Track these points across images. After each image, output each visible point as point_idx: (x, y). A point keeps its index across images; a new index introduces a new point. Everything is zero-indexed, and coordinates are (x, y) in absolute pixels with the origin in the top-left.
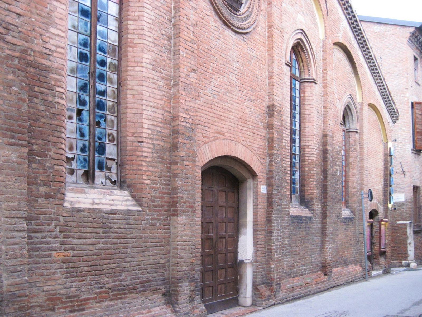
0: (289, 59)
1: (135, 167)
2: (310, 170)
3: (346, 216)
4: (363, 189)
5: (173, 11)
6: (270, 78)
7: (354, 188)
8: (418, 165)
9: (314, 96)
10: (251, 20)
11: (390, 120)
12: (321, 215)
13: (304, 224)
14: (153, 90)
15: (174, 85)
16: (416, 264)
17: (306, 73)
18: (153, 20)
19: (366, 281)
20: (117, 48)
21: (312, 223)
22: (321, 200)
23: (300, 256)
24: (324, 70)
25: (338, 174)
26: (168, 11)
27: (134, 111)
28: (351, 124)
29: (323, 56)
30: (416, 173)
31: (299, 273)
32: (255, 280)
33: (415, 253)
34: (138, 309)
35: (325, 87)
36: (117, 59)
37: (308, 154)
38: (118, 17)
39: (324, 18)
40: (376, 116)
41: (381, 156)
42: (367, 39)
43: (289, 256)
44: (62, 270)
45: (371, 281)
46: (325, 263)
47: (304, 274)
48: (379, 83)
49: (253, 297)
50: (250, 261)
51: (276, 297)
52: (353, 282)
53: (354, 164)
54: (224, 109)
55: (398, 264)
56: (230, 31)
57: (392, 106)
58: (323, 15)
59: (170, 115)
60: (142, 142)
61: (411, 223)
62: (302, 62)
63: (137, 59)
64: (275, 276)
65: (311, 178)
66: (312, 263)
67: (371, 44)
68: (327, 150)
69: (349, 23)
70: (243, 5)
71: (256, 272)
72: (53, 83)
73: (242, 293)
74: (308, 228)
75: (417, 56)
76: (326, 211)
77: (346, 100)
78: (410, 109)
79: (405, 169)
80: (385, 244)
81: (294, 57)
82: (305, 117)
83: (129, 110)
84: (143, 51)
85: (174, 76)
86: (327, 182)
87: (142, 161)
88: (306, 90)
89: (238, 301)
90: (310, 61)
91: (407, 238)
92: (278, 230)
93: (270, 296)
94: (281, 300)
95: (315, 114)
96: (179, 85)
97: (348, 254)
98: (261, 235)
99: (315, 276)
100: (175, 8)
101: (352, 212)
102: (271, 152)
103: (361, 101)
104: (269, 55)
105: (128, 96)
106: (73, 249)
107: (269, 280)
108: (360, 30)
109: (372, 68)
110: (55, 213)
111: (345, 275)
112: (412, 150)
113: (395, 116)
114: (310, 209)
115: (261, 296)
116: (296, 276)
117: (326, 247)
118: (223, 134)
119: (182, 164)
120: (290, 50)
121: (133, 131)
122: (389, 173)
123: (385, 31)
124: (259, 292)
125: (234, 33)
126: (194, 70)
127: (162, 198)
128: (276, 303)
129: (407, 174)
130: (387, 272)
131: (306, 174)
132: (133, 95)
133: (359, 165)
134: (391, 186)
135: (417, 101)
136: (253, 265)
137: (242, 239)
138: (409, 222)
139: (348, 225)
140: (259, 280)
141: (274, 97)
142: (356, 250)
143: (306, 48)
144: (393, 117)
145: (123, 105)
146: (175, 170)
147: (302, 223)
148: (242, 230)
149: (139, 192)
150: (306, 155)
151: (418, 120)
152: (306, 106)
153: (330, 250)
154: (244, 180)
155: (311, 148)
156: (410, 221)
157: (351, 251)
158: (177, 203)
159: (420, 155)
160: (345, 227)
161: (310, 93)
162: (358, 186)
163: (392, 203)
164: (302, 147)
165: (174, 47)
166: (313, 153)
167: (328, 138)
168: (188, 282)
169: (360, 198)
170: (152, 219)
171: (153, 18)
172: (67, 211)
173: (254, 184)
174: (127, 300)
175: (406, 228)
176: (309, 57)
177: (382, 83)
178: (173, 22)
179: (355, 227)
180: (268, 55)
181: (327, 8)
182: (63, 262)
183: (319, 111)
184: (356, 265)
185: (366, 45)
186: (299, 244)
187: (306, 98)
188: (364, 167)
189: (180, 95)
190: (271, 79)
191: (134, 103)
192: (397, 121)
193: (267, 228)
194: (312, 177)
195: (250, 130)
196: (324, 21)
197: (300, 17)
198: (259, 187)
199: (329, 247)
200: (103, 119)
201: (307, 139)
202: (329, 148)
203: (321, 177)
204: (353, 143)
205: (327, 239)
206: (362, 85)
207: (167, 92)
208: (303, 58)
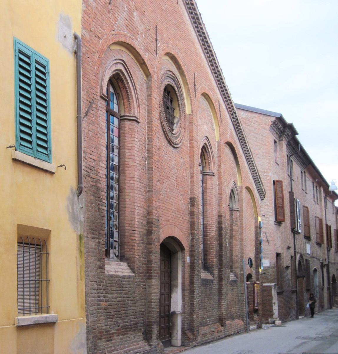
0: (105, 93)
1: (131, 247)
2: (211, 243)
3: (233, 279)
4: (243, 257)
5: (147, 141)
6: (192, 177)
7: (237, 256)
8: (279, 235)
9: (213, 186)
10: (181, 136)
11: (259, 199)
12: (218, 278)
13: (209, 285)
14: (139, 195)
15: (149, 191)
16: (280, 322)
17: (207, 168)
18: (138, 148)
19: (247, 333)
20: (118, 167)
21: (213, 285)
22: (218, 267)
23: (207, 310)
24: (219, 165)
25: (227, 246)
26: (144, 141)
27: (130, 210)
28: (234, 204)
29: (218, 154)
30: (277, 241)
31: (206, 323)
32: (184, 327)
33: (279, 312)
34: (133, 342)
35: (220, 178)
36: (118, 174)
37: (209, 230)
38: (118, 146)
39: (219, 125)
40: (250, 196)
41: (253, 229)
42: (245, 136)
43: (201, 310)
44: (104, 314)
45: (251, 333)
46: (222, 317)
47: (209, 324)
48: (252, 169)
49: (182, 339)
50: (180, 312)
51: (196, 341)
52: (238, 333)
53: (237, 236)
54: (169, 203)
55: (265, 321)
56: (171, 147)
57: (261, 187)
58: (219, 123)
59: (146, 211)
60: (135, 230)
61: (275, 285)
62: (205, 159)
63: (131, 176)
64: (196, 324)
65: (211, 250)
66: (213, 315)
67: (247, 139)
68: (222, 227)
69: (233, 124)
70: (175, 125)
71: (184, 321)
72: (102, 197)
73: (174, 336)
74: (211, 288)
75: (276, 140)
76: (222, 275)
77: (231, 185)
78: (272, 186)
79: (269, 238)
80: (258, 303)
81: (111, 90)
82: (207, 202)
83: (126, 209)
84: (135, 171)
85: (149, 185)
86: (222, 253)
87: (135, 243)
88: (208, 181)
89: (171, 342)
90: (210, 159)
91: (272, 298)
92: (197, 290)
93: (193, 339)
94: (199, 343)
95: (214, 200)
96: (152, 191)
97: (234, 310)
98: (187, 293)
99: (215, 326)
100: (148, 138)
101: (235, 276)
102: (192, 232)
103: (241, 185)
104: (191, 160)
105: (126, 200)
106: (108, 301)
107: (192, 327)
108: (241, 129)
109: (249, 160)
110: (102, 278)
111: (234, 327)
112: (275, 222)
113: (263, 194)
114: (212, 273)
115: (188, 339)
116: (205, 326)
117: (222, 303)
118: (169, 221)
119: (154, 245)
120: (106, 83)
121: (129, 223)
122: (259, 242)
123: (251, 118)
124: (187, 335)
125: (173, 148)
126: (159, 180)
127: (143, 267)
128: (197, 344)
129: (271, 242)
130: (259, 327)
131: (208, 246)
132: (129, 199)
133: (240, 237)
134: (260, 253)
135: (278, 179)
136: (182, 316)
137: (173, 296)
138: (273, 284)
139: (234, 286)
140: (186, 327)
141: (195, 192)
142: (238, 307)
143: (208, 149)
144: (261, 195)
145: (122, 205)
146: (150, 248)
147: (208, 284)
148: (174, 289)
149: (133, 263)
150: (208, 231)
151: (279, 196)
152: (208, 193)
153: (224, 306)
154: (176, 252)
155: (212, 226)
156: (274, 284)
157: (236, 307)
158: (152, 271)
159: (280, 226)
160: (232, 288)
161: (210, 183)
162: (239, 254)
163: (262, 269)
164: (205, 225)
165: (148, 165)
166: (213, 231)
167: (223, 218)
168: (156, 325)
169: (241, 264)
170: (139, 282)
171: (139, 147)
172: (106, 277)
173: (182, 256)
174: (128, 335)
175: (271, 290)
176: (210, 156)
177: (254, 169)
178: (147, 148)
179: (238, 288)
180: (190, 160)
181: (221, 117)
182: (105, 309)
183: (216, 197)
184: (239, 320)
185: (244, 140)
186: (206, 301)
187: (208, 187)
188: (244, 239)
189: (153, 199)
190: (192, 178)
191: (130, 204)
192: (264, 199)
193: (190, 288)
194: (212, 249)
195: (181, 217)
196: (219, 127)
197: (205, 127)
198: (186, 258)
199: (224, 303)
200: (113, 215)
201: (208, 219)
202: (223, 226)
203: (218, 248)
204: (236, 219)
205: (223, 298)
206: (242, 173)
207: (145, 196)
208: (205, 157)
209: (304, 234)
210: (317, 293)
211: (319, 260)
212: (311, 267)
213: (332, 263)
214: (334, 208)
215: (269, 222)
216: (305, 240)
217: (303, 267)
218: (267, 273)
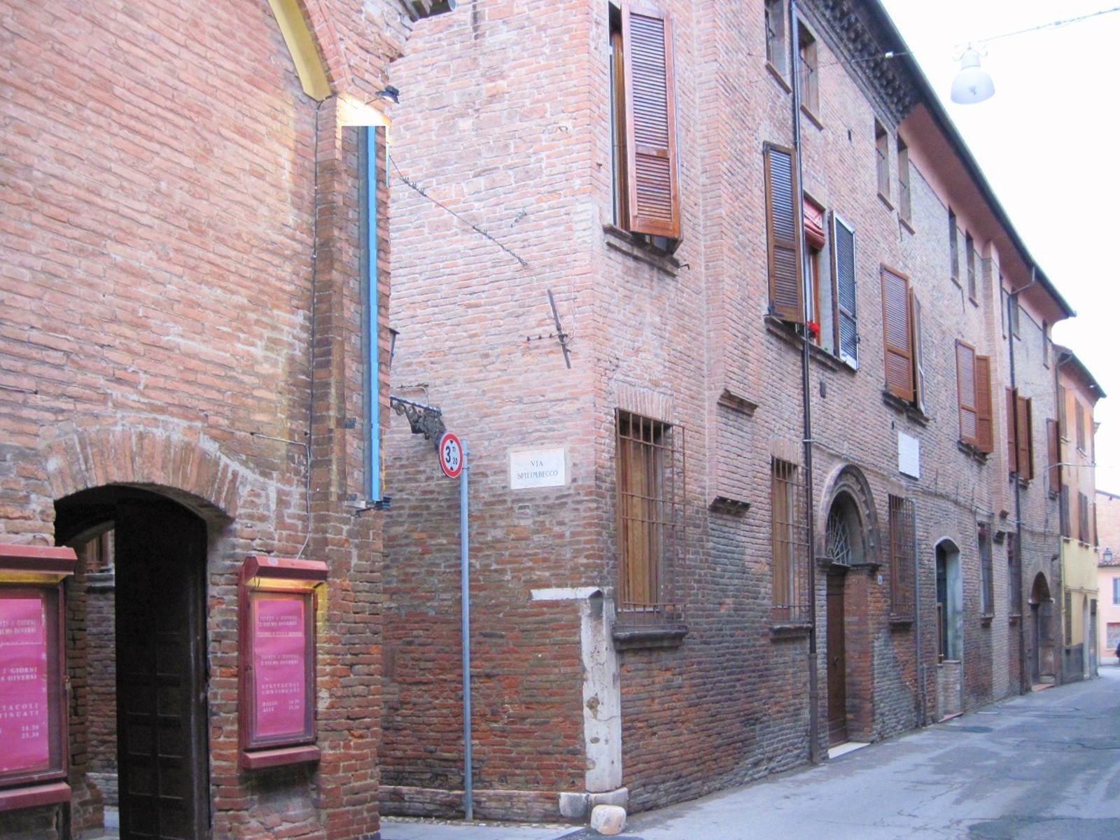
129: (580, 347)
138: (586, 592)
175: (575, 626)
209: (881, 387)
210: (957, 637)
211: (974, 513)
212: (919, 533)
213: (1032, 533)
214: (1050, 348)
215: (570, 229)
216: (889, 416)
217: (867, 528)
218: (557, 529)
